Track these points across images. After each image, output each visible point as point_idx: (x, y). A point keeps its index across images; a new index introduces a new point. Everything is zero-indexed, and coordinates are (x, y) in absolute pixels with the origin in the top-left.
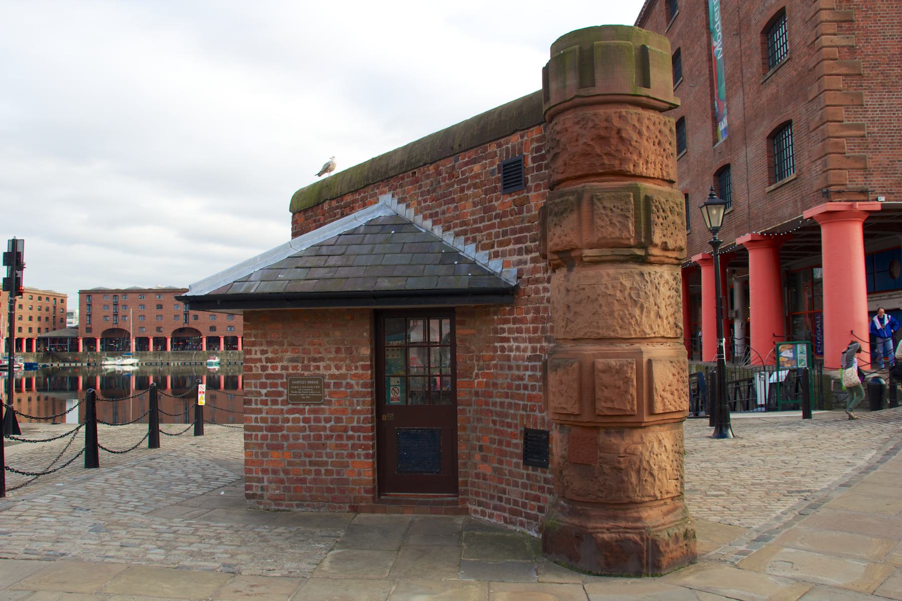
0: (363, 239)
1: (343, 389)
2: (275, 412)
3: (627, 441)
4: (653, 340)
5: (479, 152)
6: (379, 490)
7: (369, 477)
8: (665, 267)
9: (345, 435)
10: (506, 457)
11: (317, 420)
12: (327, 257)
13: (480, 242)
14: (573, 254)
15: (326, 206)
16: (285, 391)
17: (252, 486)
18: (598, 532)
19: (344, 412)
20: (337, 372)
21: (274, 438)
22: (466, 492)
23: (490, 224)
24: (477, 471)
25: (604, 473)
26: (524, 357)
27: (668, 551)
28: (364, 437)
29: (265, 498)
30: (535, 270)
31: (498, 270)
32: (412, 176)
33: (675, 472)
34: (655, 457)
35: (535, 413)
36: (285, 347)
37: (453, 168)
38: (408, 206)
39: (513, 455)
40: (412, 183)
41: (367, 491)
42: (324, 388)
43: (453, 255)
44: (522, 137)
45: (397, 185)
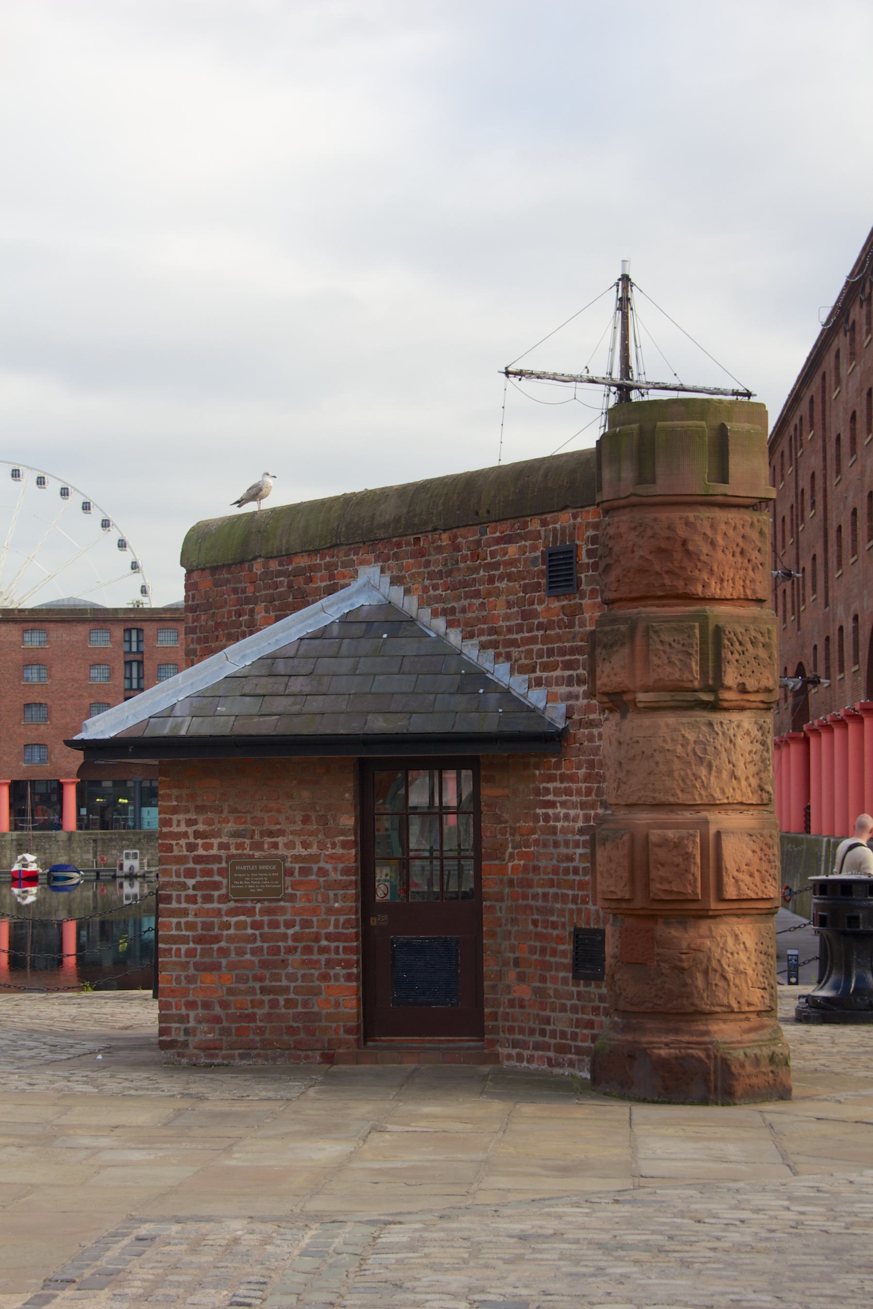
0: (340, 648)
1: (313, 877)
2: (208, 913)
3: (691, 934)
4: (728, 807)
5: (516, 526)
6: (365, 1029)
7: (351, 1009)
8: (747, 714)
9: (315, 946)
10: (551, 971)
11: (274, 924)
12: (287, 678)
13: (516, 661)
14: (626, 698)
15: (258, 568)
16: (225, 881)
17: (170, 1028)
18: (654, 1048)
19: (314, 911)
20: (304, 853)
21: (205, 953)
22: (495, 1030)
23: (531, 637)
24: (511, 997)
25: (663, 974)
26: (574, 828)
27: (743, 1073)
28: (344, 948)
29: (191, 1046)
30: (588, 709)
31: (541, 705)
32: (415, 544)
33: (761, 979)
34: (729, 955)
35: (588, 906)
36: (225, 814)
37: (478, 543)
38: (407, 592)
39: (559, 967)
40: (414, 555)
41: (348, 1031)
42: (285, 875)
43: (479, 677)
44: (575, 517)
45: (389, 554)
